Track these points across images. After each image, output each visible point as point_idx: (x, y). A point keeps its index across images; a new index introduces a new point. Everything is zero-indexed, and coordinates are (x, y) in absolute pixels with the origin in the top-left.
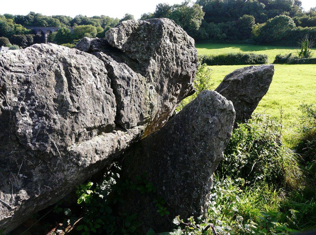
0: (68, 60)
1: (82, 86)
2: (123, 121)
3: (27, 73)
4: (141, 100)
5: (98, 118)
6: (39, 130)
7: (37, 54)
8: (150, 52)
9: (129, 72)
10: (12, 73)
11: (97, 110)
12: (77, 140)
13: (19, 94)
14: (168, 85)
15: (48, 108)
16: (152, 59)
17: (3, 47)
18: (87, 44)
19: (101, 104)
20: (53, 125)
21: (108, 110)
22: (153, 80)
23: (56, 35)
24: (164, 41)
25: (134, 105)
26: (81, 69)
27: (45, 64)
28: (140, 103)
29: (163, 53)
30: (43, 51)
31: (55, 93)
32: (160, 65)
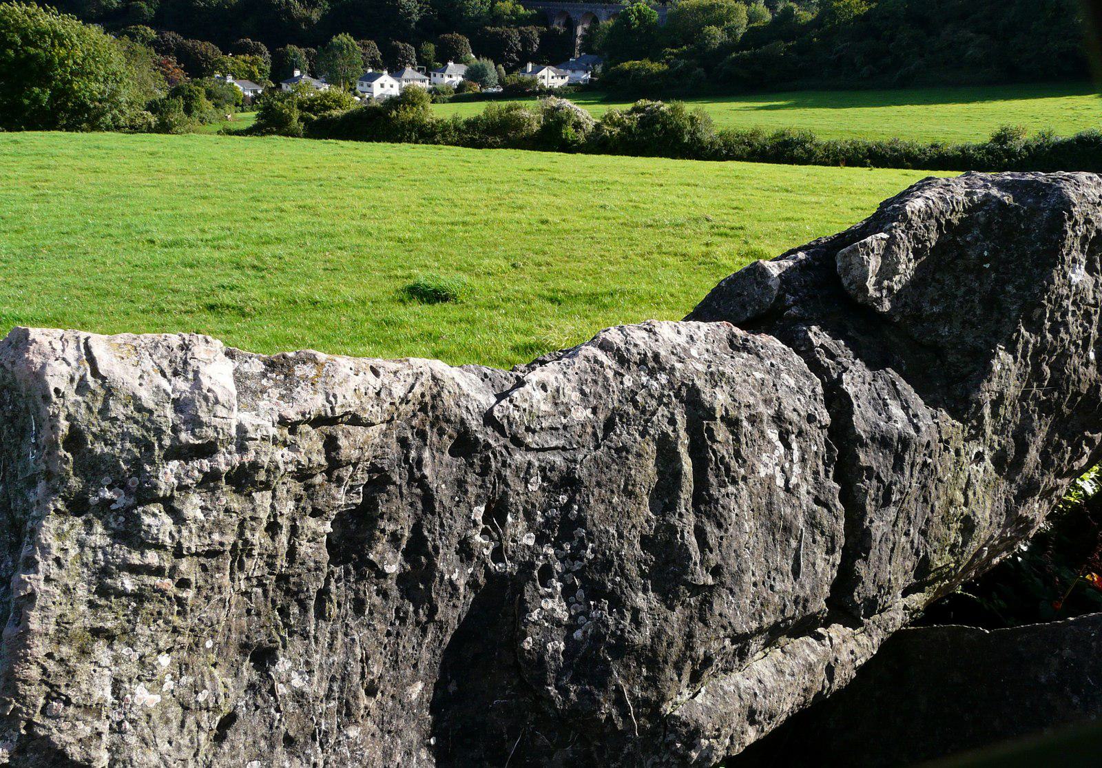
0: (706, 397)
1: (737, 489)
2: (856, 598)
3: (574, 449)
4: (932, 511)
5: (776, 599)
6: (585, 646)
7: (610, 374)
8: (998, 321)
9: (907, 414)
10: (530, 457)
11: (776, 569)
12: (695, 678)
13: (542, 520)
14: (1048, 441)
15: (622, 571)
16: (1001, 353)
17: (451, 64)
18: (768, 287)
19: (794, 544)
20: (629, 632)
21: (814, 565)
22: (989, 430)
23: (612, 29)
24: (1064, 276)
25: (907, 534)
26: (745, 423)
27: (631, 410)
28: (928, 521)
29: (1048, 324)
30: (628, 361)
31: (651, 514)
32: (1029, 369)
